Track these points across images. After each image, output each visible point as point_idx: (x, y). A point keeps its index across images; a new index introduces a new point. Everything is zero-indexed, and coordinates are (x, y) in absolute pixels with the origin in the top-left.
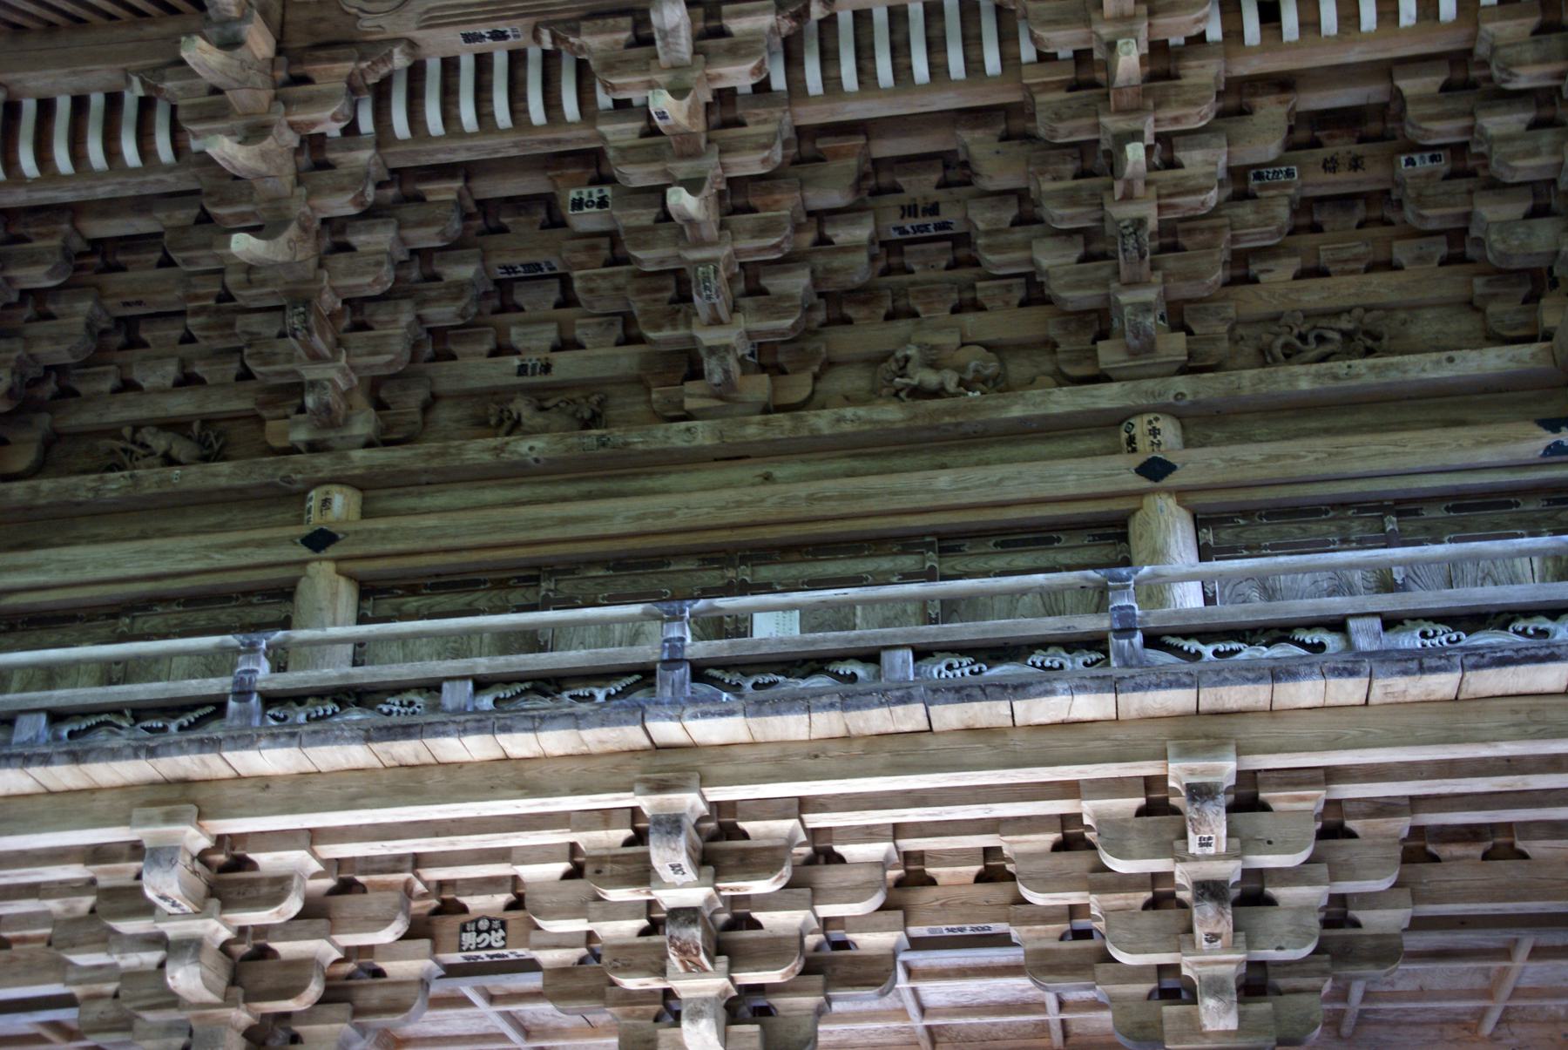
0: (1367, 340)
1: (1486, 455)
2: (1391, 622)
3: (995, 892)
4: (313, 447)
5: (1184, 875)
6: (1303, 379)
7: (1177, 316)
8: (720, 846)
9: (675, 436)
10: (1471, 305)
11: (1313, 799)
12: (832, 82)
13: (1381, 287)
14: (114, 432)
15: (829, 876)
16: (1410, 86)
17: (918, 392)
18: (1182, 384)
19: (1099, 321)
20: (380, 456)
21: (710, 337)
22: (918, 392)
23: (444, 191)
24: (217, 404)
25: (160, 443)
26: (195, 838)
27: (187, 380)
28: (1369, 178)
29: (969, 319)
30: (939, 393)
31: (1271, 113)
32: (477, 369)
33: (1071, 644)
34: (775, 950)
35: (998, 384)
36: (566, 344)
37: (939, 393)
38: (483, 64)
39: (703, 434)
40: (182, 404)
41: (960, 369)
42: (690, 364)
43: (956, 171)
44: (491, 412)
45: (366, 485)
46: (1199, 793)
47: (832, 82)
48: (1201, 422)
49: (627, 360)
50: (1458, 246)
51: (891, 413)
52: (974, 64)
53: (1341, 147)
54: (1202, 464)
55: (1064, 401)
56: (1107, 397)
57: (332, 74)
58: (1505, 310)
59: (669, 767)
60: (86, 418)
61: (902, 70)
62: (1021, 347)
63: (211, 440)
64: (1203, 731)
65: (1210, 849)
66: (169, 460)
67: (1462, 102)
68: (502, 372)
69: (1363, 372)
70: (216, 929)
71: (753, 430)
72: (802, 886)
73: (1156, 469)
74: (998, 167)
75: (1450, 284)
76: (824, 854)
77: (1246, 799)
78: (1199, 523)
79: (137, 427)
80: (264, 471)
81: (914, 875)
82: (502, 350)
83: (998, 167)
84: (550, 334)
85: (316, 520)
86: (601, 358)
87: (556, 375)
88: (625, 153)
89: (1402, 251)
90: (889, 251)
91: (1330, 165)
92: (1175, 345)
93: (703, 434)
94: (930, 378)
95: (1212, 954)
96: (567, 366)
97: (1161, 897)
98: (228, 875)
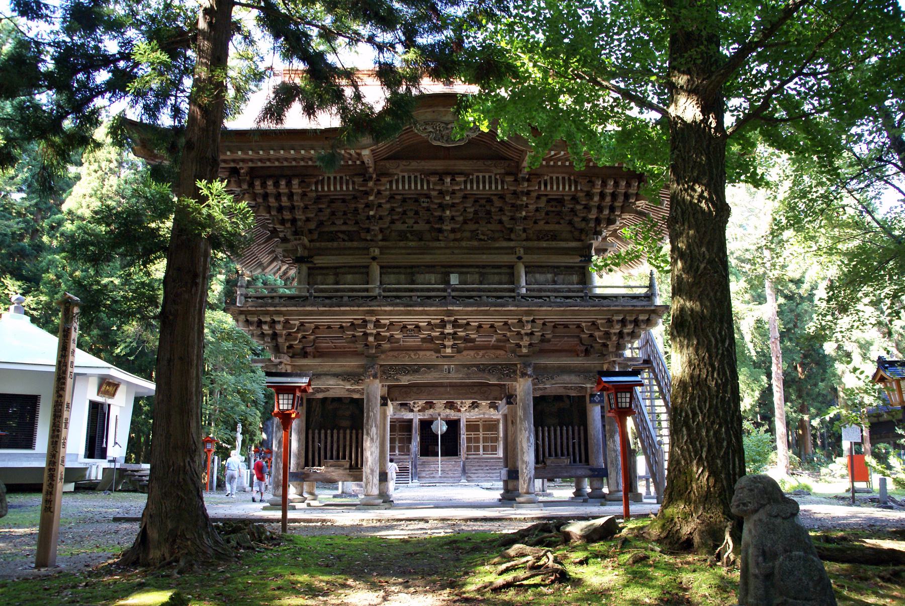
0: (554, 238)
1: (571, 261)
2: (556, 297)
3: (492, 330)
4: (371, 240)
5: (523, 332)
6: (544, 244)
7: (524, 230)
8: (455, 324)
9: (437, 244)
10: (571, 232)
11: (542, 321)
12: (472, 187)
13: (557, 227)
14: (331, 232)
15: (469, 327)
16: (566, 198)
17: (481, 240)
18: (524, 243)
19: (511, 230)
20: (384, 243)
21: (445, 228)
22: (481, 240)
23: (399, 197)
24: (350, 229)
25: (341, 236)
26: (374, 319)
27: (345, 223)
28: (558, 209)
29: (489, 225)
30: (484, 240)
31: (544, 199)
32: (399, 226)
33: (510, 297)
34: (460, 338)
35: (494, 239)
36: (416, 223)
37: (484, 240)
38: (409, 177)
39: (442, 244)
40: (344, 228)
41: (487, 235)
42: (440, 231)
43: (489, 201)
44: (403, 236)
45: (381, 248)
46: (527, 322)
47: (472, 187)
48: (528, 250)
49: (427, 227)
50: (570, 223)
51: (476, 243)
52: (496, 187)
53: (554, 203)
54: (527, 258)
55: (505, 244)
56: (512, 244)
57: (384, 180)
58: (576, 234)
59: (450, 313)
60: (326, 229)
61: (484, 187)
62: (497, 231)
63: (351, 236)
64: (528, 313)
65: (528, 328)
66: (344, 240)
67: (573, 202)
68: (403, 227)
69: (554, 244)
70: (374, 332)
71: (451, 244)
72: (466, 330)
73: (520, 258)
74: (498, 203)
75: (569, 228)
76: (468, 324)
77: (533, 321)
78: (526, 267)
79: (337, 232)
80: (362, 244)
81: (480, 326)
82: (404, 223)
83: (498, 203)
84: (413, 221)
85: (372, 255)
86: (422, 226)
87: (415, 228)
88: (435, 197)
89: (562, 221)
90: (476, 212)
91: (552, 207)
92: (524, 235)
93: (442, 244)
94: (482, 237)
95: (525, 342)
96: (416, 227)
97: (519, 333)
98: (377, 324)
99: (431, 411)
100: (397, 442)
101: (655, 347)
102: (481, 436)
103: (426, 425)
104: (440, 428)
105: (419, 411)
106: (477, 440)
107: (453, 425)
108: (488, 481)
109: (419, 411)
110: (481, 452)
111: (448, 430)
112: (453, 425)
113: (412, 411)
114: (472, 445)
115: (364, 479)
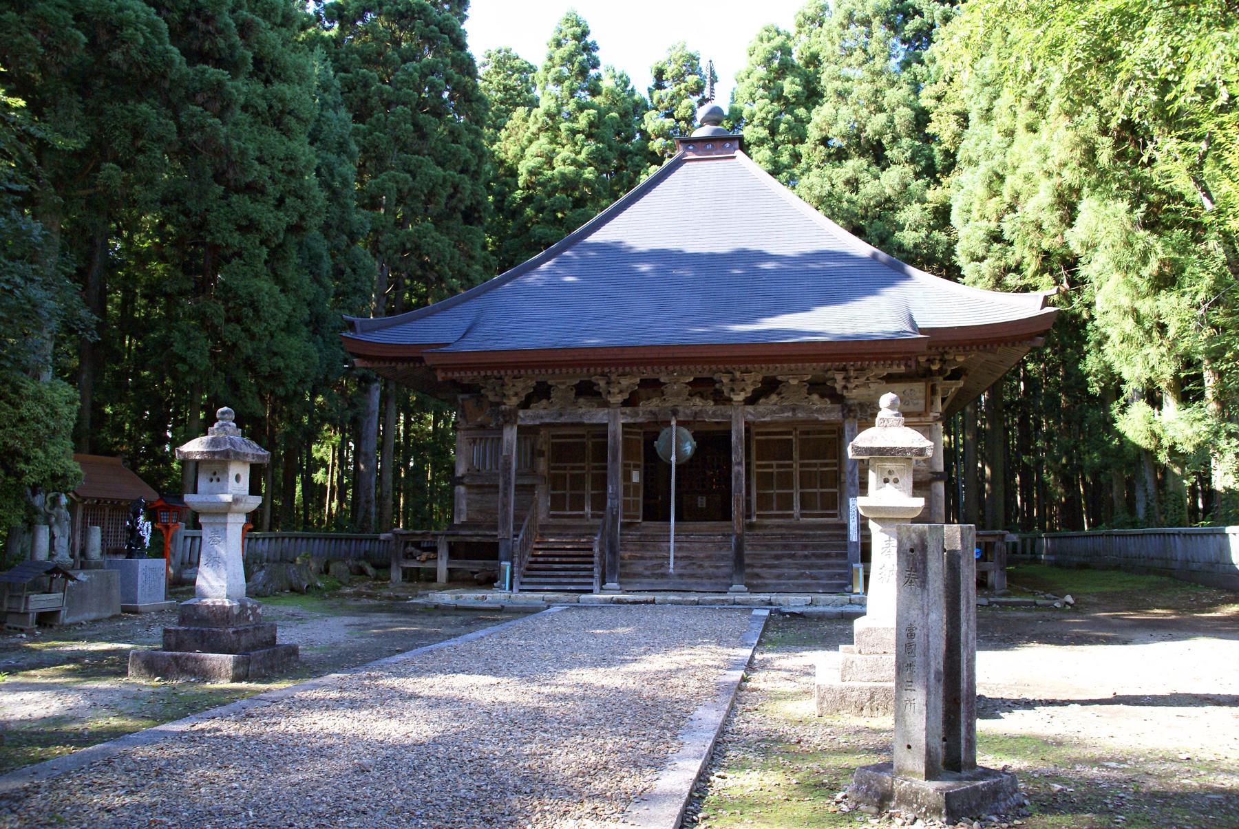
99: (654, 404)
100: (588, 486)
101: (997, 737)
102: (796, 469)
103: (645, 442)
104: (679, 446)
105: (625, 403)
106: (786, 480)
107: (714, 443)
108: (804, 589)
109: (625, 403)
110: (796, 510)
111: (697, 451)
112: (714, 443)
113: (606, 404)
114: (774, 491)
115: (645, 523)
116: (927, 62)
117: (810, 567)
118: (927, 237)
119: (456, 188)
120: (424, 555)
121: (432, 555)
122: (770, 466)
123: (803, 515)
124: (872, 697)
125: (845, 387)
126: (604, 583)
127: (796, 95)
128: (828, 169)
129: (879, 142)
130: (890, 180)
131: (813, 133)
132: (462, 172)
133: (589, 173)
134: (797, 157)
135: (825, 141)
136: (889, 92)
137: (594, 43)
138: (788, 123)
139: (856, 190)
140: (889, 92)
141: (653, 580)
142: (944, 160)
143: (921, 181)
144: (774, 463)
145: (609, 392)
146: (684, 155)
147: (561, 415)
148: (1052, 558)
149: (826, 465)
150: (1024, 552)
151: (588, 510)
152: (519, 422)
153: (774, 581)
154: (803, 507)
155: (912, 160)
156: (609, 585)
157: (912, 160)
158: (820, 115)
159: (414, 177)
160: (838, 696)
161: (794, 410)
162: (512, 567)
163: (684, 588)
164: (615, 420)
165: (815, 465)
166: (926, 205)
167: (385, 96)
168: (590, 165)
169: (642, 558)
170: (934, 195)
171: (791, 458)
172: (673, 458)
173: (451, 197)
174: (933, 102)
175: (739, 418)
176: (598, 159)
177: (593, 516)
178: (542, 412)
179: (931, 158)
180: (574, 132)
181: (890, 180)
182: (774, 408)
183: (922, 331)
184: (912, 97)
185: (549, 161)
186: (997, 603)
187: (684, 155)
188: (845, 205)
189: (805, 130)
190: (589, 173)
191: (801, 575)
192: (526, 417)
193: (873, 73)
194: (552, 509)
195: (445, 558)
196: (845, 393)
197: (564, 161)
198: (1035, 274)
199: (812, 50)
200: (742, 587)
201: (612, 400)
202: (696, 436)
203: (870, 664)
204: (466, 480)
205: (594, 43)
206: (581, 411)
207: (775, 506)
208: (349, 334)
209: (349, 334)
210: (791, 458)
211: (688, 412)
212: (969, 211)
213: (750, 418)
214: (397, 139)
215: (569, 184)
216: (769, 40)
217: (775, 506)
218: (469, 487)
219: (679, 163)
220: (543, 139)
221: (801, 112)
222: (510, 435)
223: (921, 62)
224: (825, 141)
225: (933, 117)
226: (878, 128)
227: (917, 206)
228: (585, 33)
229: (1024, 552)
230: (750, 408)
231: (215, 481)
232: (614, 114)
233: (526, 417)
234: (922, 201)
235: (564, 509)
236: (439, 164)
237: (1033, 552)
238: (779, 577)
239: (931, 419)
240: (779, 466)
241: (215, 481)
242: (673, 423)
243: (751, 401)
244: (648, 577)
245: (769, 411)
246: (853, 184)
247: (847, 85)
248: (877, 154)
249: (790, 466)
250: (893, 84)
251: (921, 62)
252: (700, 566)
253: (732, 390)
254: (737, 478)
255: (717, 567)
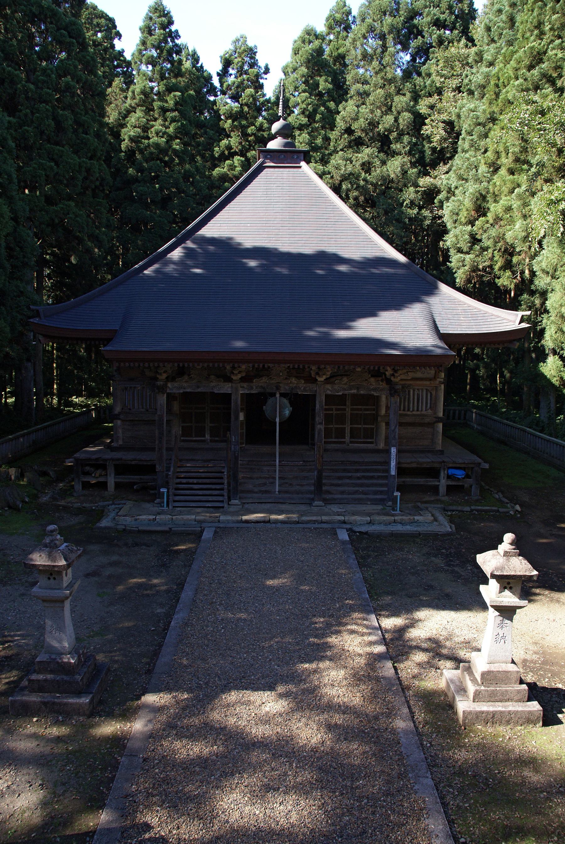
102: (348, 412)
103: (255, 403)
105: (243, 380)
107: (302, 405)
109: (243, 380)
110: (347, 439)
111: (292, 414)
112: (302, 405)
116: (423, 75)
117: (362, 485)
118: (418, 213)
119: (88, 170)
120: (98, 472)
121: (103, 473)
122: (332, 410)
123: (351, 442)
124: (493, 717)
125: (393, 375)
126: (229, 499)
127: (329, 92)
128: (349, 154)
129: (387, 137)
130: (394, 167)
131: (340, 124)
132: (91, 158)
133: (176, 145)
134: (327, 139)
135: (349, 131)
136: (396, 99)
137: (177, 31)
138: (322, 114)
139: (368, 171)
140: (396, 99)
141: (260, 495)
142: (432, 155)
143: (415, 170)
144: (334, 407)
145: (233, 373)
146: (263, 162)
147: (198, 387)
148: (479, 428)
149: (367, 410)
150: (459, 419)
151: (208, 437)
152: (168, 391)
153: (340, 496)
154: (351, 437)
155: (410, 153)
156: (233, 502)
157: (410, 153)
158: (348, 108)
159: (57, 164)
160: (474, 717)
161: (358, 389)
162: (168, 492)
163: (281, 501)
164: (237, 390)
165: (361, 410)
166: (418, 189)
167: (30, 94)
168: (177, 138)
169: (251, 478)
170: (425, 181)
171: (345, 405)
172: (277, 420)
173: (86, 178)
174: (428, 111)
175: (322, 390)
176: (181, 133)
177: (211, 441)
178: (185, 385)
179: (422, 152)
180: (164, 110)
181: (394, 167)
182: (345, 387)
183: (443, 337)
184: (412, 103)
185: (146, 129)
186: (477, 510)
187: (263, 162)
188: (362, 183)
189: (335, 120)
190: (176, 145)
191: (356, 492)
192: (173, 387)
193: (385, 80)
194: (183, 435)
195: (113, 475)
196: (392, 379)
197: (157, 134)
198: (500, 269)
199: (340, 51)
200: (321, 503)
201: (234, 378)
202: (291, 404)
203: (490, 693)
204: (122, 417)
205: (177, 31)
206: (213, 384)
207: (333, 436)
208: (36, 320)
209: (36, 320)
210: (345, 405)
211: (287, 388)
212: (457, 214)
213: (329, 392)
214: (42, 133)
215: (162, 150)
216: (310, 42)
217: (333, 436)
218: (123, 421)
219: (260, 169)
220: (139, 113)
221: (332, 105)
222: (162, 399)
223: (419, 74)
224: (349, 131)
225: (427, 121)
226: (387, 126)
227: (412, 189)
228: (171, 23)
229: (459, 419)
230: (329, 386)
231: (52, 580)
232: (192, 92)
233: (173, 387)
234: (416, 185)
235: (192, 436)
236: (76, 152)
237: (465, 418)
238: (342, 493)
239: (437, 382)
240: (337, 410)
241: (52, 580)
242: (278, 395)
243: (327, 381)
244: (256, 493)
245: (339, 388)
246: (367, 167)
247: (366, 87)
248: (384, 144)
249: (345, 410)
250: (399, 92)
251: (419, 74)
252: (291, 484)
253: (317, 374)
254: (319, 434)
255: (302, 485)
